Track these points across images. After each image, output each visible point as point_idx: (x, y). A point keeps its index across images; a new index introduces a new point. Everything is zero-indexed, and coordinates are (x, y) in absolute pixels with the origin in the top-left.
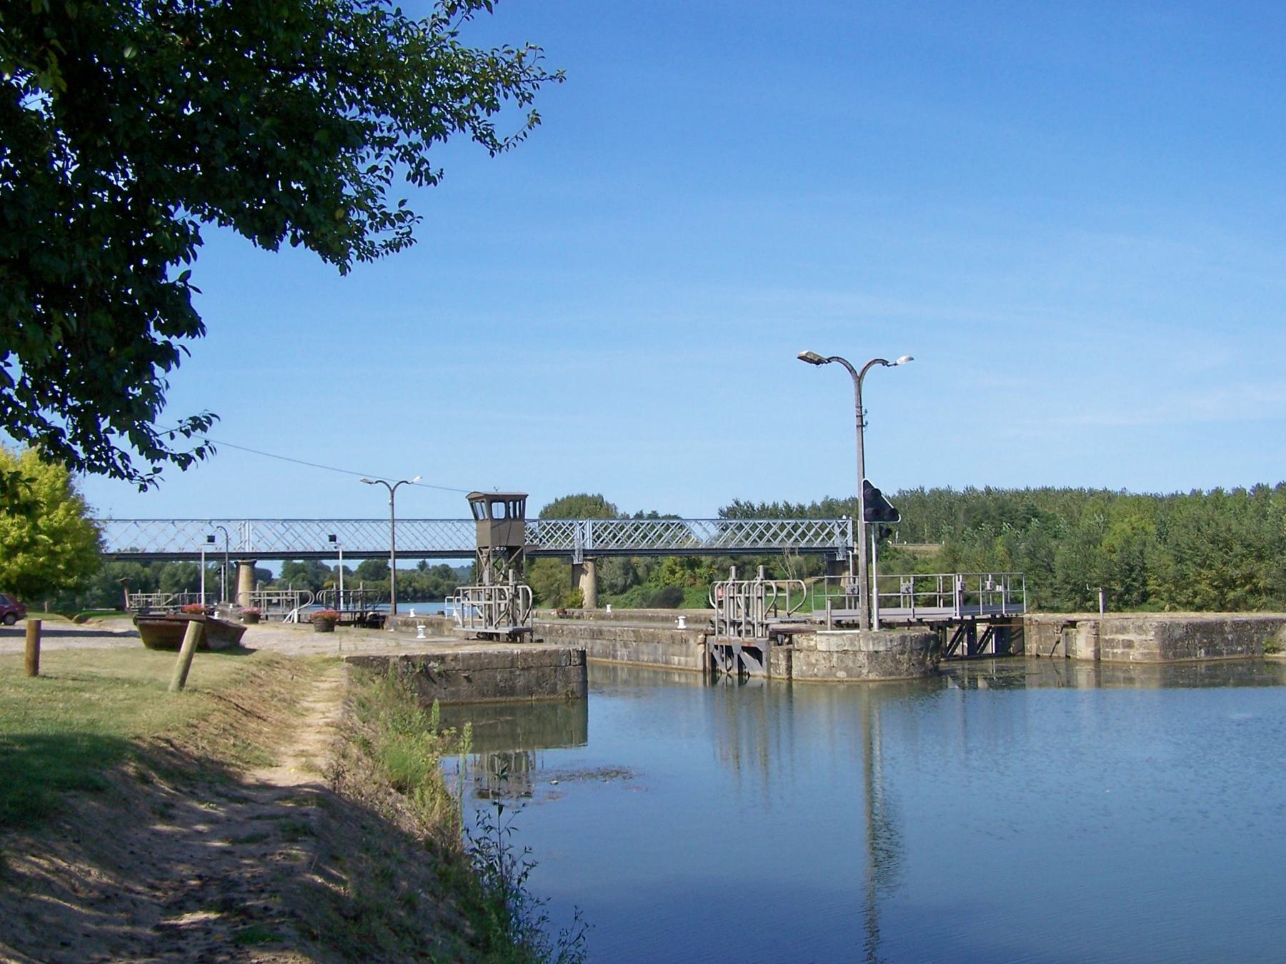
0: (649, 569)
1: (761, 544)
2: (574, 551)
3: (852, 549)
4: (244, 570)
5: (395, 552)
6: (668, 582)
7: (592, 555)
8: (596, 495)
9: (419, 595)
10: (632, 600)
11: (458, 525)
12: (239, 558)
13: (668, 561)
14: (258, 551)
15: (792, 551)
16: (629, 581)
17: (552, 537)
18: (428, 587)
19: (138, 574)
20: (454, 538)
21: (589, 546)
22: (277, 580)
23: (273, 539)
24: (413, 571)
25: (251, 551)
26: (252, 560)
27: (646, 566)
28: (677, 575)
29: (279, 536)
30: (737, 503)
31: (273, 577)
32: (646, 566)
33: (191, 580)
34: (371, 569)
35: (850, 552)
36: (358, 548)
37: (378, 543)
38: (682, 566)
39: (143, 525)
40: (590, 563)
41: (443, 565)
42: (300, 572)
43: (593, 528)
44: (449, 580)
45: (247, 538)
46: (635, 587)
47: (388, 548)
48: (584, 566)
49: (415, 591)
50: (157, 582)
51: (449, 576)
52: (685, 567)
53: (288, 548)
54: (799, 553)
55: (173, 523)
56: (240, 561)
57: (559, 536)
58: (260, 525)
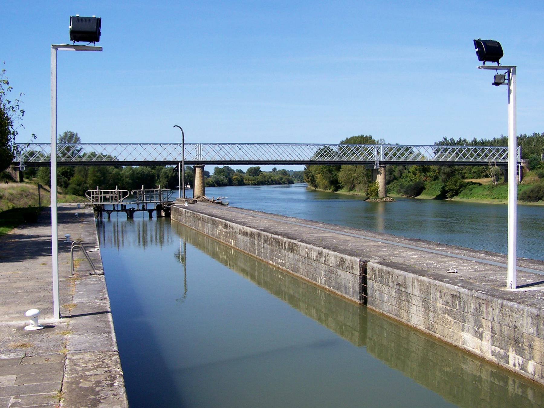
0: (401, 173)
1: (394, 159)
2: (374, 161)
3: (520, 163)
4: (198, 170)
5: (185, 161)
6: (412, 179)
7: (383, 164)
8: (368, 136)
9: (274, 182)
10: (394, 188)
11: (295, 147)
12: (195, 164)
13: (412, 168)
14: (206, 160)
15: (493, 164)
16: (392, 178)
17: (354, 153)
18: (278, 179)
19: (149, 172)
20: (292, 154)
21: (382, 159)
22: (212, 176)
23: (214, 154)
24: (270, 172)
25: (202, 160)
26: (385, 165)
27: (399, 170)
28: (417, 175)
29: (217, 152)
30: (445, 139)
31: (210, 174)
32: (399, 170)
33: (173, 175)
34: (253, 171)
35: (519, 165)
36: (212, 159)
37: (251, 156)
38: (420, 171)
39: (145, 146)
40: (383, 168)
41: (250, 168)
42: (222, 172)
43: (384, 149)
44: (286, 176)
45: (199, 153)
46: (395, 181)
47: (180, 158)
48: (380, 170)
49: (272, 180)
50: (158, 176)
51: (286, 174)
52: (422, 172)
53: (212, 159)
54: (497, 165)
55: (160, 145)
56: (196, 166)
57: (340, 153)
58: (207, 147)
